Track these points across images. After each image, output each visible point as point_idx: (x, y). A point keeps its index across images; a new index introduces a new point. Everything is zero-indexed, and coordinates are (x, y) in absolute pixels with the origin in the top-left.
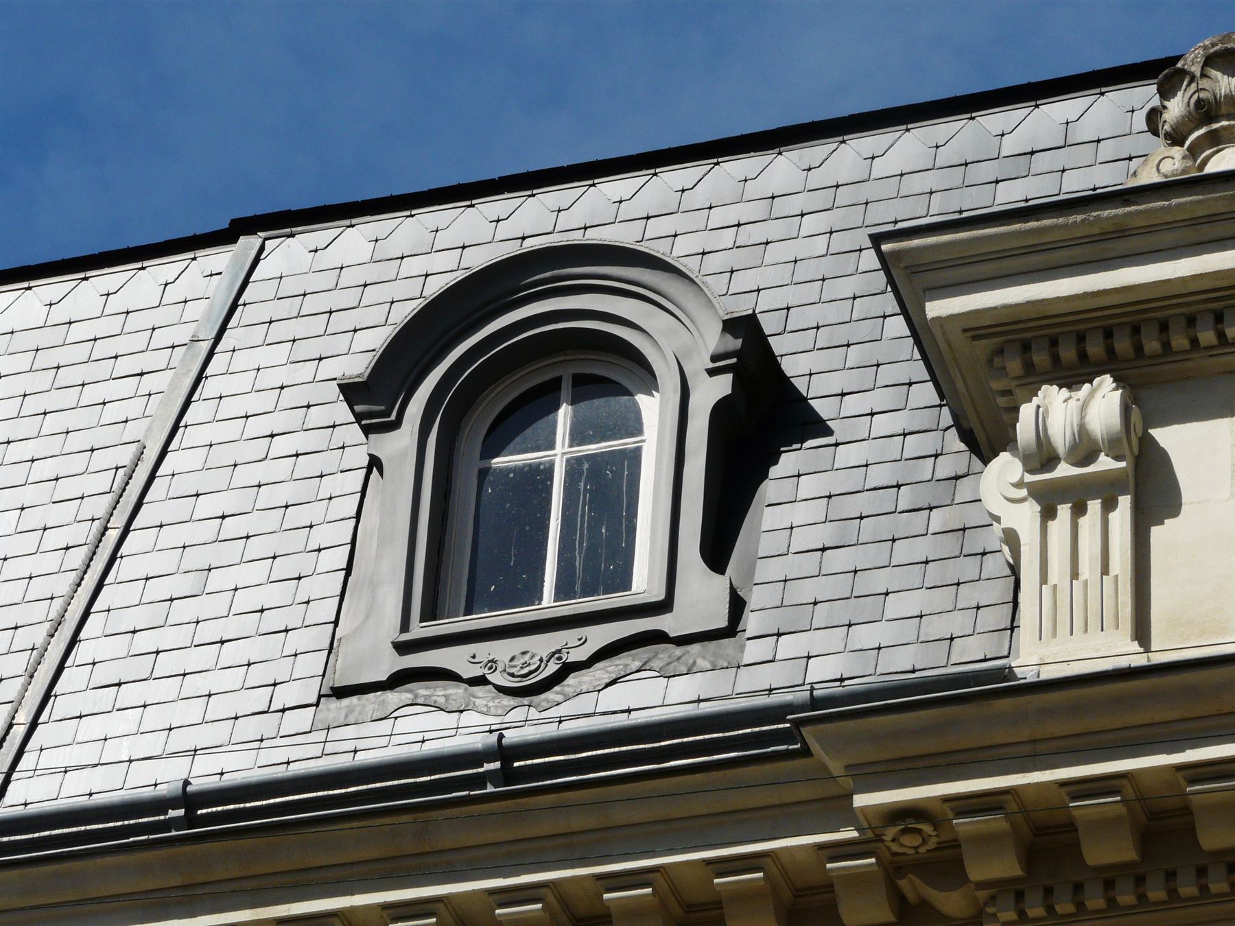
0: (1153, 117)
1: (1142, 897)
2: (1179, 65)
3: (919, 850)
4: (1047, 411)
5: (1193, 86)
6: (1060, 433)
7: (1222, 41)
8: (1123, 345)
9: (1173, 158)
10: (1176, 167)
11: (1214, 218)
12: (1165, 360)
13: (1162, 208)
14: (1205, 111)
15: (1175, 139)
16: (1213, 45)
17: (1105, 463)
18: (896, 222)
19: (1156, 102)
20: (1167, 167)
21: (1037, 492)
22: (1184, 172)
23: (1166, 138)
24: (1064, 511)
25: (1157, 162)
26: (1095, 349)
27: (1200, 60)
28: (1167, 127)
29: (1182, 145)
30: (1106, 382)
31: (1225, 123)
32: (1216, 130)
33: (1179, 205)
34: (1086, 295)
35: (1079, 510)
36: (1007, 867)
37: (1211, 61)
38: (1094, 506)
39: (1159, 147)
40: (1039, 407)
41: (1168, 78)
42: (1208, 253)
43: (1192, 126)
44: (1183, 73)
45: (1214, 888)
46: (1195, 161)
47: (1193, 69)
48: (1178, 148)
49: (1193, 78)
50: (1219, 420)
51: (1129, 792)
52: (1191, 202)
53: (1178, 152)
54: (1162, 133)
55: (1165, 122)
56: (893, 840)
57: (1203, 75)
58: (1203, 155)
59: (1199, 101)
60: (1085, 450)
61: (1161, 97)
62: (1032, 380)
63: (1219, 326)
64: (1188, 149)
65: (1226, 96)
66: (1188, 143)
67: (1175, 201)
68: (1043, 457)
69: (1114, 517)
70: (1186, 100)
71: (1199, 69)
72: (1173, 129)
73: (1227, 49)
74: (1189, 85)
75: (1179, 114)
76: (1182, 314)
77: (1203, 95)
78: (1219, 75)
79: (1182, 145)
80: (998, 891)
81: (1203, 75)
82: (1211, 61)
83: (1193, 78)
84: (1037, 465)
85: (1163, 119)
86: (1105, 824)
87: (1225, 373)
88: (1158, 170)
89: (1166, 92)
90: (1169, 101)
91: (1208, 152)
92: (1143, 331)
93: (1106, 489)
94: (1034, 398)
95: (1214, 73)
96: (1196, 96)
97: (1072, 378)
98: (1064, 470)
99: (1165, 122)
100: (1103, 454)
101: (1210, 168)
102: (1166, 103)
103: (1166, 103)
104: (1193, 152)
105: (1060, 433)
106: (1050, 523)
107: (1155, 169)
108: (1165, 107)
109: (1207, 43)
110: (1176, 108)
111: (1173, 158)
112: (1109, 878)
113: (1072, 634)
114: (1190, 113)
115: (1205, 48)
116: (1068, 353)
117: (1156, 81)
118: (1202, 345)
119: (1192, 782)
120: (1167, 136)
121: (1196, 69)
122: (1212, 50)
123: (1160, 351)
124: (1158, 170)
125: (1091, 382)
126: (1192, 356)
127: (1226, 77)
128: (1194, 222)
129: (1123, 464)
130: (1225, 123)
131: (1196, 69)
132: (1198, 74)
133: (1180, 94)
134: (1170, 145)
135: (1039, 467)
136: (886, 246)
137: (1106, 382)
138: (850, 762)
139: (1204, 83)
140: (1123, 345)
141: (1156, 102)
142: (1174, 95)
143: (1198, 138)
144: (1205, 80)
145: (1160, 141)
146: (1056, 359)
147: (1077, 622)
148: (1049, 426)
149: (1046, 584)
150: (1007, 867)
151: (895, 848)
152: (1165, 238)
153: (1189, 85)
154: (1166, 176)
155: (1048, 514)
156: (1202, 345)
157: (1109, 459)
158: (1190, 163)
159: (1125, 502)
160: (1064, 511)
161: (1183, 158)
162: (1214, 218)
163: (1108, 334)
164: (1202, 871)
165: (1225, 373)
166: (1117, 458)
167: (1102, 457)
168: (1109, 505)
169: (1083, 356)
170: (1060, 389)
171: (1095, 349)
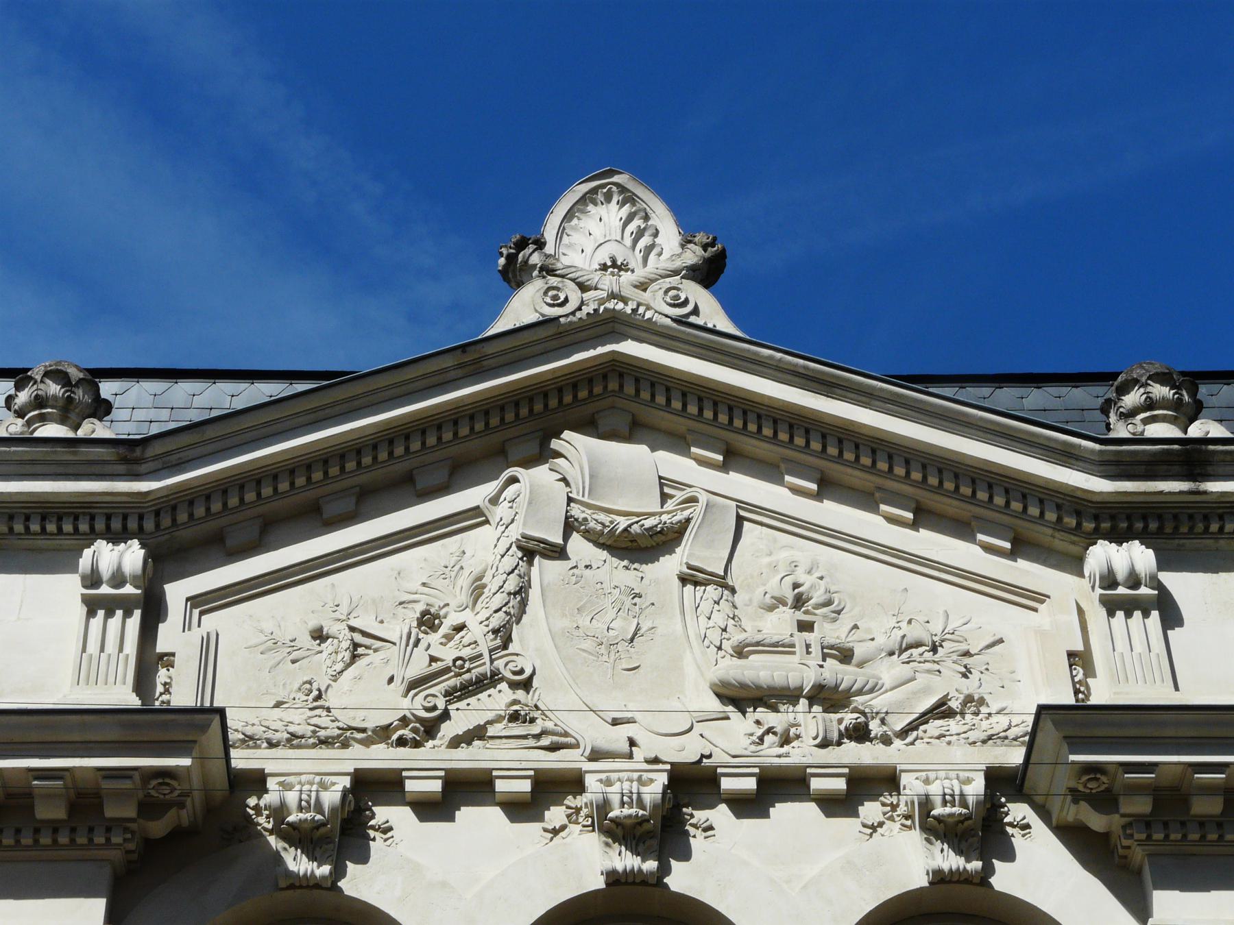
0: (9, 400)
1: (73, 841)
2: (29, 374)
3: (167, 797)
4: (99, 553)
5: (35, 386)
6: (106, 569)
7: (56, 364)
8: (149, 525)
9: (17, 425)
10: (18, 429)
11: (34, 462)
12: (58, 538)
13: (5, 452)
14: (39, 402)
15: (20, 414)
16: (50, 366)
17: (129, 589)
18: (129, 435)
19: (12, 392)
20: (13, 429)
21: (87, 600)
22: (21, 433)
23: (14, 413)
24: (101, 613)
25: (7, 425)
26: (132, 524)
27: (42, 373)
28: (16, 407)
29: (23, 418)
30: (135, 544)
31: (49, 410)
32: (44, 413)
33: (15, 452)
34: (1145, 493)
35: (110, 614)
36: (60, 813)
37: (47, 374)
38: (119, 613)
39: (10, 417)
40: (95, 552)
41: (21, 379)
42: (27, 481)
43: (31, 408)
44: (31, 378)
45: (24, 841)
46: (29, 428)
47: (36, 377)
48: (21, 419)
49: (35, 382)
50: (17, 575)
51: (69, 780)
52: (22, 451)
53: (20, 422)
54: (13, 410)
55: (15, 404)
56: (153, 788)
57: (42, 381)
58: (35, 426)
59: (37, 396)
60: (118, 579)
61: (16, 389)
62: (91, 537)
63: (27, 523)
64: (26, 421)
65: (53, 395)
66: (26, 418)
67: (13, 449)
68: (92, 580)
69: (130, 621)
70: (30, 393)
71: (40, 378)
72: (19, 409)
73: (57, 370)
74: (32, 385)
75: (24, 401)
76: (7, 513)
77: (40, 392)
78: (51, 383)
79: (23, 418)
80: (1135, 820)
81: (42, 381)
82: (47, 374)
83: (35, 382)
84: (89, 583)
85: (15, 402)
86: (49, 796)
87: (26, 549)
88: (7, 430)
89: (19, 387)
90: (20, 392)
91: (37, 425)
92: (112, 519)
93: (126, 604)
94: (92, 547)
95: (48, 381)
96: (36, 392)
97: (116, 537)
98: (105, 589)
99: (15, 404)
100: (128, 584)
101: (37, 434)
102: (18, 393)
103: (18, 393)
104: (29, 423)
105: (106, 569)
106: (128, 620)
107: (5, 429)
108: (17, 396)
109: (47, 364)
110: (23, 397)
111: (17, 425)
112: (1202, 823)
113: (78, 684)
114: (31, 401)
115: (46, 367)
116: (116, 525)
117: (14, 380)
118: (15, 532)
119: (36, 778)
120: (16, 412)
121: (38, 378)
122: (49, 369)
123: (39, 531)
124: (7, 430)
125: (1127, 542)
126: (8, 537)
127: (54, 384)
128: (22, 463)
129: (139, 592)
130: (49, 410)
131: (38, 378)
132: (39, 380)
133: (27, 390)
134: (16, 417)
135: (90, 585)
136: (695, 449)
137: (135, 544)
138: (1068, 734)
139: (41, 386)
140: (149, 525)
141: (12, 392)
142: (23, 390)
143: (34, 416)
144: (42, 385)
145: (11, 414)
146: (108, 527)
147: (111, 679)
148: (99, 565)
149: (85, 652)
150: (60, 813)
151: (153, 793)
152: (71, 470)
153: (32, 385)
154: (11, 434)
155: (91, 613)
156: (15, 532)
157: (131, 587)
158: (26, 429)
159: (137, 613)
160: (101, 613)
161: (23, 426)
162: (34, 462)
163: (108, 517)
164: (37, 831)
165: (26, 549)
166: (136, 587)
167: (1120, 587)
168: (128, 614)
169: (125, 527)
170: (108, 543)
171: (132, 524)
